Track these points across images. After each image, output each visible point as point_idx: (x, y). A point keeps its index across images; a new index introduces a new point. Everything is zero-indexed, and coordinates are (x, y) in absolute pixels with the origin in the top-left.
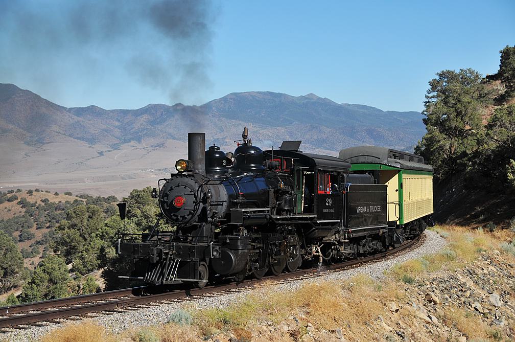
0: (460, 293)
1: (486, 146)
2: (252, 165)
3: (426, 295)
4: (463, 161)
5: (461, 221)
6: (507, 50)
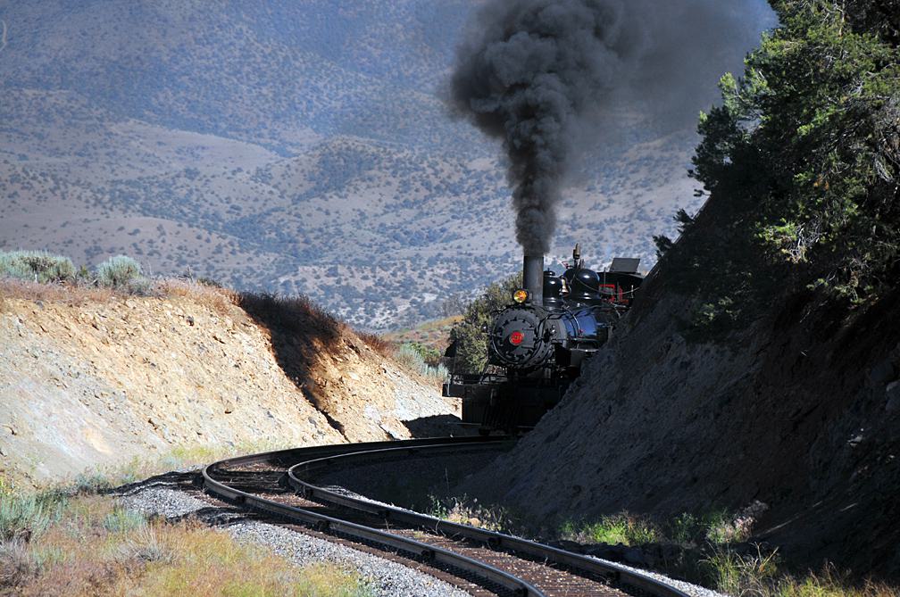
2: (586, 294)
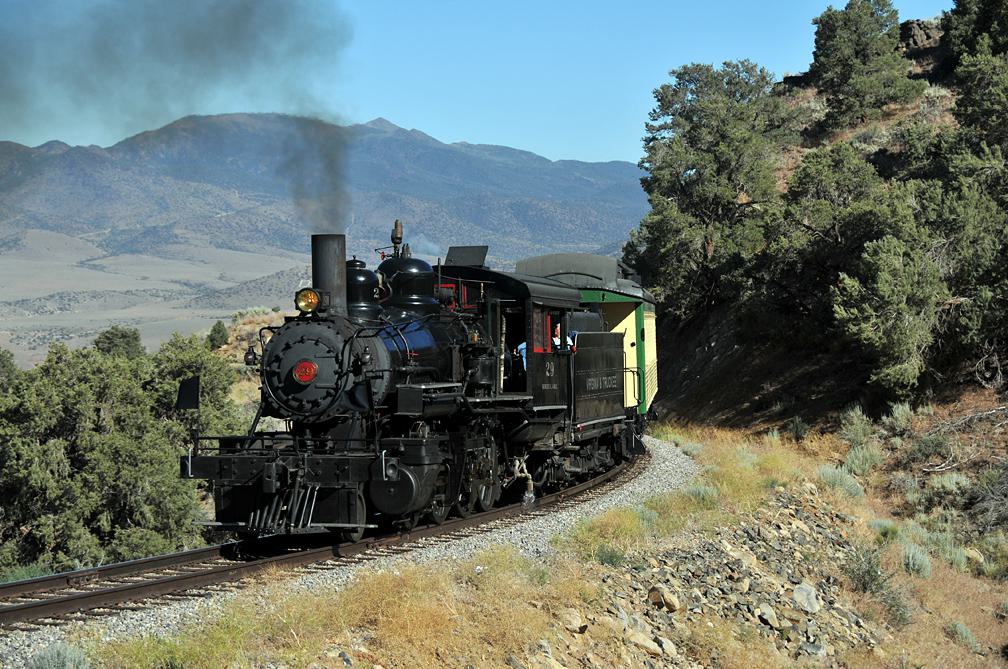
0: (726, 585)
1: (784, 242)
2: (415, 297)
3: (651, 591)
4: (733, 276)
5: (729, 415)
6: (829, 16)
